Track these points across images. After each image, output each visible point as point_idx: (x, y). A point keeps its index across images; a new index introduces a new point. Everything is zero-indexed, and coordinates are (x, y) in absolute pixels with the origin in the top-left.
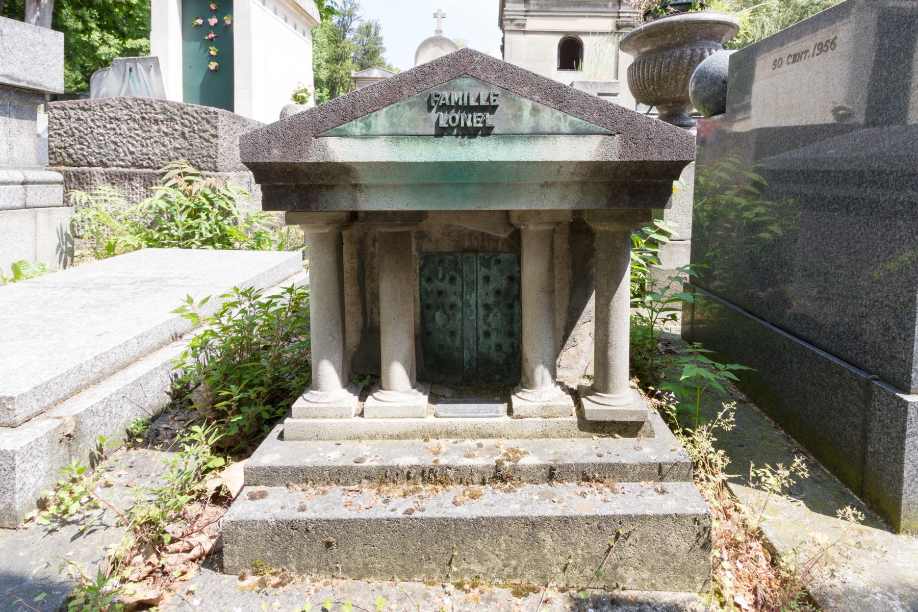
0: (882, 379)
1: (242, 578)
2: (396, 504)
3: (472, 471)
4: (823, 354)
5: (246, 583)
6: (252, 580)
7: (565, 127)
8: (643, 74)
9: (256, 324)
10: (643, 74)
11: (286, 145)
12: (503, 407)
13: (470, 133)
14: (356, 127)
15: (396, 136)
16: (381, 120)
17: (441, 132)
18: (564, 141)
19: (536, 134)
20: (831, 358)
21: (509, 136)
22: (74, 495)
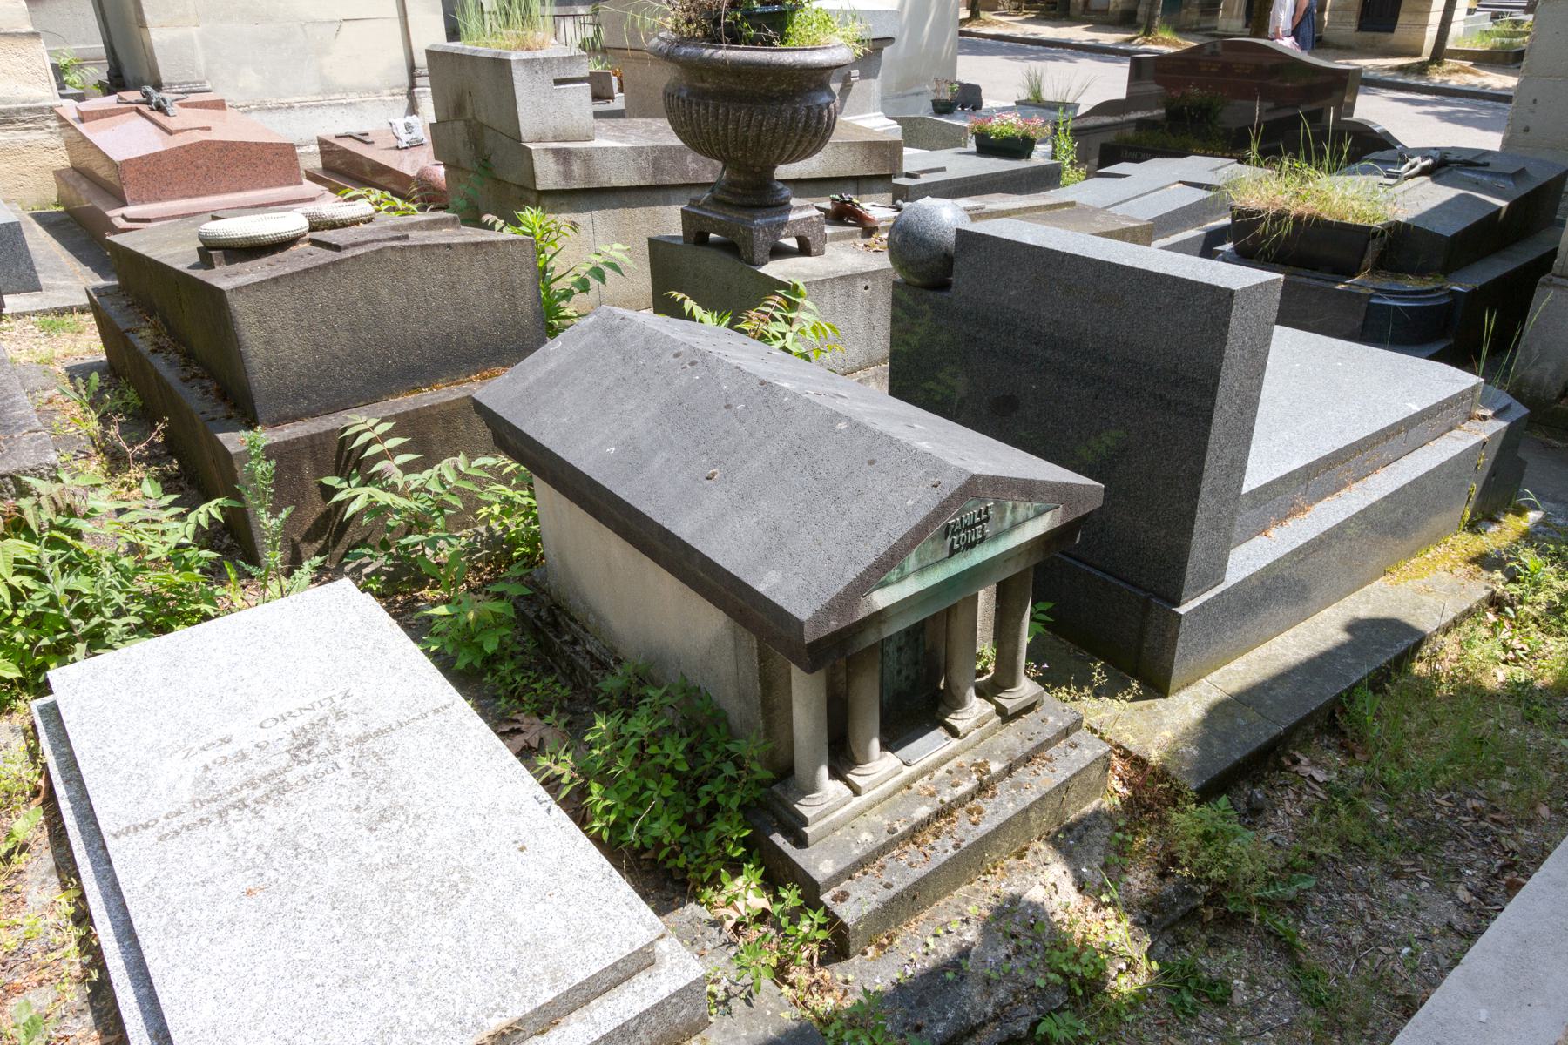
0: (1159, 596)
1: (865, 953)
2: (943, 849)
3: (964, 796)
4: (1100, 574)
5: (870, 954)
6: (871, 951)
7: (1031, 513)
8: (725, 128)
9: (102, 614)
10: (725, 128)
11: (841, 614)
12: (940, 733)
13: (970, 546)
14: (894, 574)
15: (922, 570)
16: (911, 562)
17: (953, 552)
18: (1029, 524)
19: (1015, 526)
20: (1109, 578)
21: (997, 536)
22: (963, 961)
